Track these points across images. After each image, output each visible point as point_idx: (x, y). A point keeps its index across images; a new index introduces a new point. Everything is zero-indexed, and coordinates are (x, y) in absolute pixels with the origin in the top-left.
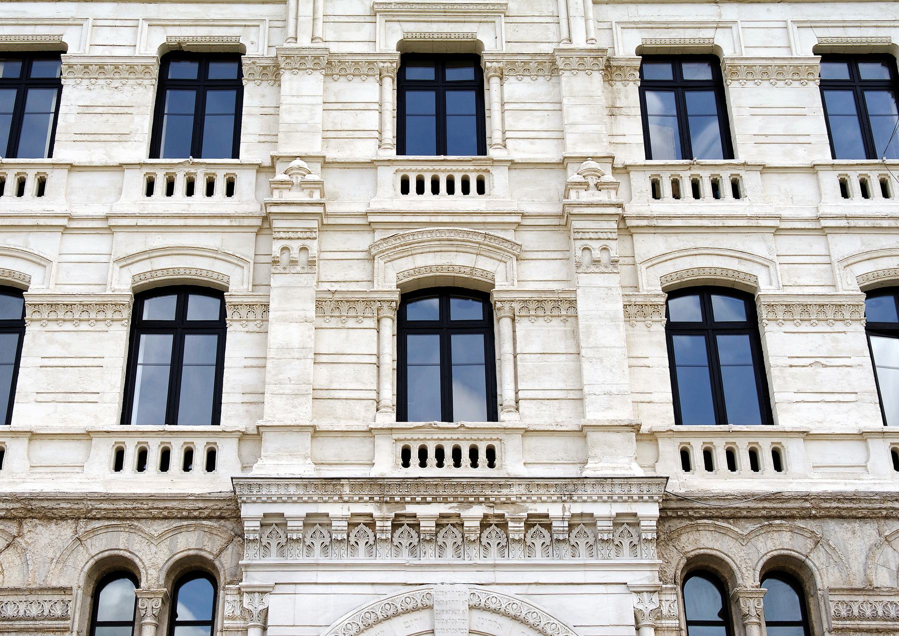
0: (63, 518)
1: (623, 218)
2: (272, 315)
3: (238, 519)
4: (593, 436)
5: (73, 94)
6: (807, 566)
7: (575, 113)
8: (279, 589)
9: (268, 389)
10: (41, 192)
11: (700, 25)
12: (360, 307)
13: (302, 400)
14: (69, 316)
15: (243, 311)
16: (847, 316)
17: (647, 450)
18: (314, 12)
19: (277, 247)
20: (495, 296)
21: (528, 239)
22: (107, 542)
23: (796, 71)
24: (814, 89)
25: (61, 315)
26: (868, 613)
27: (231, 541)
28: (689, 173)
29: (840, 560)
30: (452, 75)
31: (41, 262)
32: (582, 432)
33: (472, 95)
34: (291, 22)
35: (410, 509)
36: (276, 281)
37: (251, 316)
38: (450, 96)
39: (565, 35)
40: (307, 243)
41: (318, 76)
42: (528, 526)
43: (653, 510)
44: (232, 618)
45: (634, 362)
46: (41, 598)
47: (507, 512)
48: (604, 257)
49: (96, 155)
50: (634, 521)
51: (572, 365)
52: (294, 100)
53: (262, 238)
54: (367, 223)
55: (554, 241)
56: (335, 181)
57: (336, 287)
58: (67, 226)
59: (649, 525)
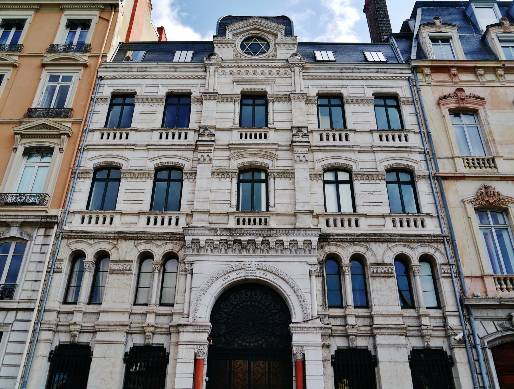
0: (131, 239)
1: (310, 147)
2: (197, 176)
3: (185, 241)
4: (299, 216)
5: (138, 108)
6: (364, 257)
7: (295, 113)
8: (196, 262)
9: (195, 200)
10: (127, 138)
11: (337, 87)
12: (226, 175)
13: (206, 203)
14: (134, 177)
15: (189, 176)
16: (380, 178)
17: (315, 220)
18: (214, 82)
19: (199, 155)
20: (269, 171)
21: (280, 153)
22: (143, 247)
23: (367, 102)
24: (372, 107)
25: (132, 176)
26: (383, 271)
27: (182, 247)
28: (332, 133)
29: (373, 254)
30: (258, 102)
31: (126, 159)
32: (295, 215)
33: (264, 107)
34: (207, 85)
35: (239, 238)
36: (199, 166)
37: (191, 177)
38: (257, 108)
39: (294, 89)
40: (209, 154)
41: (215, 102)
42: (276, 243)
43: (317, 239)
44: (182, 271)
45: (312, 192)
46: (123, 264)
47: (270, 239)
48: (304, 159)
49: (145, 126)
50: (310, 242)
51: (293, 193)
52: (207, 109)
53: (195, 153)
54: (229, 147)
55: (288, 154)
56: (218, 134)
57: (218, 168)
58: (134, 147)
59: (315, 244)
